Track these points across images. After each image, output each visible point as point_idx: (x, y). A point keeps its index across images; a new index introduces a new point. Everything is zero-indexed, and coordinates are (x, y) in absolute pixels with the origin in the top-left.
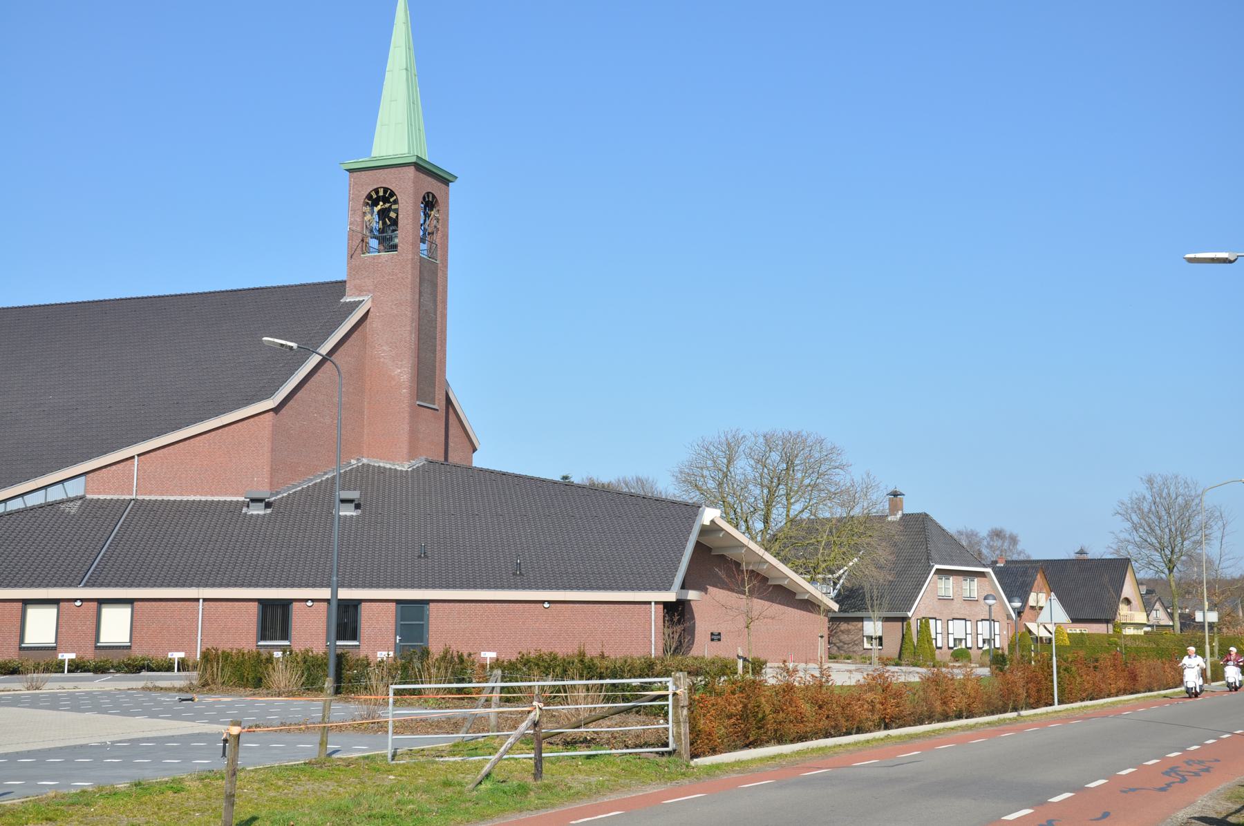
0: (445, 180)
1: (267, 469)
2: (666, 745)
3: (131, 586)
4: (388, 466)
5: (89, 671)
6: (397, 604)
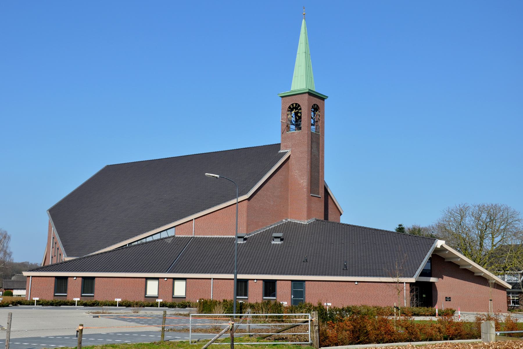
0: (322, 98)
1: (245, 224)
2: (308, 341)
3: (185, 273)
4: (299, 222)
5: (167, 307)
6: (292, 281)
